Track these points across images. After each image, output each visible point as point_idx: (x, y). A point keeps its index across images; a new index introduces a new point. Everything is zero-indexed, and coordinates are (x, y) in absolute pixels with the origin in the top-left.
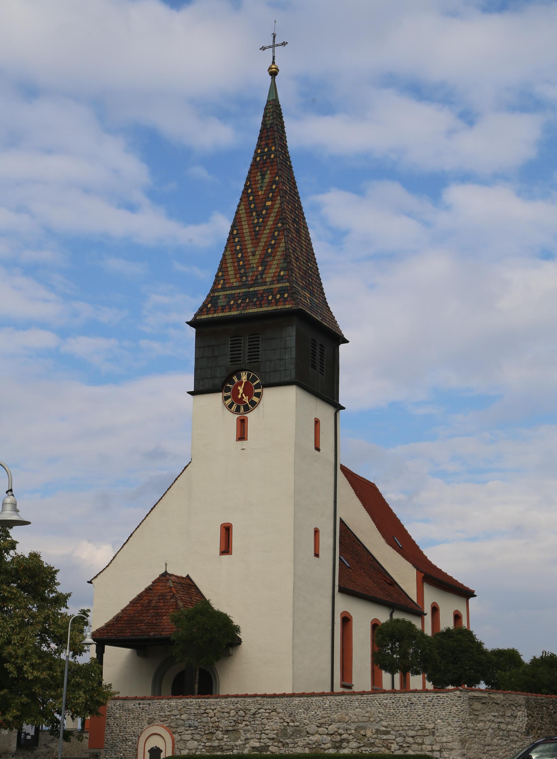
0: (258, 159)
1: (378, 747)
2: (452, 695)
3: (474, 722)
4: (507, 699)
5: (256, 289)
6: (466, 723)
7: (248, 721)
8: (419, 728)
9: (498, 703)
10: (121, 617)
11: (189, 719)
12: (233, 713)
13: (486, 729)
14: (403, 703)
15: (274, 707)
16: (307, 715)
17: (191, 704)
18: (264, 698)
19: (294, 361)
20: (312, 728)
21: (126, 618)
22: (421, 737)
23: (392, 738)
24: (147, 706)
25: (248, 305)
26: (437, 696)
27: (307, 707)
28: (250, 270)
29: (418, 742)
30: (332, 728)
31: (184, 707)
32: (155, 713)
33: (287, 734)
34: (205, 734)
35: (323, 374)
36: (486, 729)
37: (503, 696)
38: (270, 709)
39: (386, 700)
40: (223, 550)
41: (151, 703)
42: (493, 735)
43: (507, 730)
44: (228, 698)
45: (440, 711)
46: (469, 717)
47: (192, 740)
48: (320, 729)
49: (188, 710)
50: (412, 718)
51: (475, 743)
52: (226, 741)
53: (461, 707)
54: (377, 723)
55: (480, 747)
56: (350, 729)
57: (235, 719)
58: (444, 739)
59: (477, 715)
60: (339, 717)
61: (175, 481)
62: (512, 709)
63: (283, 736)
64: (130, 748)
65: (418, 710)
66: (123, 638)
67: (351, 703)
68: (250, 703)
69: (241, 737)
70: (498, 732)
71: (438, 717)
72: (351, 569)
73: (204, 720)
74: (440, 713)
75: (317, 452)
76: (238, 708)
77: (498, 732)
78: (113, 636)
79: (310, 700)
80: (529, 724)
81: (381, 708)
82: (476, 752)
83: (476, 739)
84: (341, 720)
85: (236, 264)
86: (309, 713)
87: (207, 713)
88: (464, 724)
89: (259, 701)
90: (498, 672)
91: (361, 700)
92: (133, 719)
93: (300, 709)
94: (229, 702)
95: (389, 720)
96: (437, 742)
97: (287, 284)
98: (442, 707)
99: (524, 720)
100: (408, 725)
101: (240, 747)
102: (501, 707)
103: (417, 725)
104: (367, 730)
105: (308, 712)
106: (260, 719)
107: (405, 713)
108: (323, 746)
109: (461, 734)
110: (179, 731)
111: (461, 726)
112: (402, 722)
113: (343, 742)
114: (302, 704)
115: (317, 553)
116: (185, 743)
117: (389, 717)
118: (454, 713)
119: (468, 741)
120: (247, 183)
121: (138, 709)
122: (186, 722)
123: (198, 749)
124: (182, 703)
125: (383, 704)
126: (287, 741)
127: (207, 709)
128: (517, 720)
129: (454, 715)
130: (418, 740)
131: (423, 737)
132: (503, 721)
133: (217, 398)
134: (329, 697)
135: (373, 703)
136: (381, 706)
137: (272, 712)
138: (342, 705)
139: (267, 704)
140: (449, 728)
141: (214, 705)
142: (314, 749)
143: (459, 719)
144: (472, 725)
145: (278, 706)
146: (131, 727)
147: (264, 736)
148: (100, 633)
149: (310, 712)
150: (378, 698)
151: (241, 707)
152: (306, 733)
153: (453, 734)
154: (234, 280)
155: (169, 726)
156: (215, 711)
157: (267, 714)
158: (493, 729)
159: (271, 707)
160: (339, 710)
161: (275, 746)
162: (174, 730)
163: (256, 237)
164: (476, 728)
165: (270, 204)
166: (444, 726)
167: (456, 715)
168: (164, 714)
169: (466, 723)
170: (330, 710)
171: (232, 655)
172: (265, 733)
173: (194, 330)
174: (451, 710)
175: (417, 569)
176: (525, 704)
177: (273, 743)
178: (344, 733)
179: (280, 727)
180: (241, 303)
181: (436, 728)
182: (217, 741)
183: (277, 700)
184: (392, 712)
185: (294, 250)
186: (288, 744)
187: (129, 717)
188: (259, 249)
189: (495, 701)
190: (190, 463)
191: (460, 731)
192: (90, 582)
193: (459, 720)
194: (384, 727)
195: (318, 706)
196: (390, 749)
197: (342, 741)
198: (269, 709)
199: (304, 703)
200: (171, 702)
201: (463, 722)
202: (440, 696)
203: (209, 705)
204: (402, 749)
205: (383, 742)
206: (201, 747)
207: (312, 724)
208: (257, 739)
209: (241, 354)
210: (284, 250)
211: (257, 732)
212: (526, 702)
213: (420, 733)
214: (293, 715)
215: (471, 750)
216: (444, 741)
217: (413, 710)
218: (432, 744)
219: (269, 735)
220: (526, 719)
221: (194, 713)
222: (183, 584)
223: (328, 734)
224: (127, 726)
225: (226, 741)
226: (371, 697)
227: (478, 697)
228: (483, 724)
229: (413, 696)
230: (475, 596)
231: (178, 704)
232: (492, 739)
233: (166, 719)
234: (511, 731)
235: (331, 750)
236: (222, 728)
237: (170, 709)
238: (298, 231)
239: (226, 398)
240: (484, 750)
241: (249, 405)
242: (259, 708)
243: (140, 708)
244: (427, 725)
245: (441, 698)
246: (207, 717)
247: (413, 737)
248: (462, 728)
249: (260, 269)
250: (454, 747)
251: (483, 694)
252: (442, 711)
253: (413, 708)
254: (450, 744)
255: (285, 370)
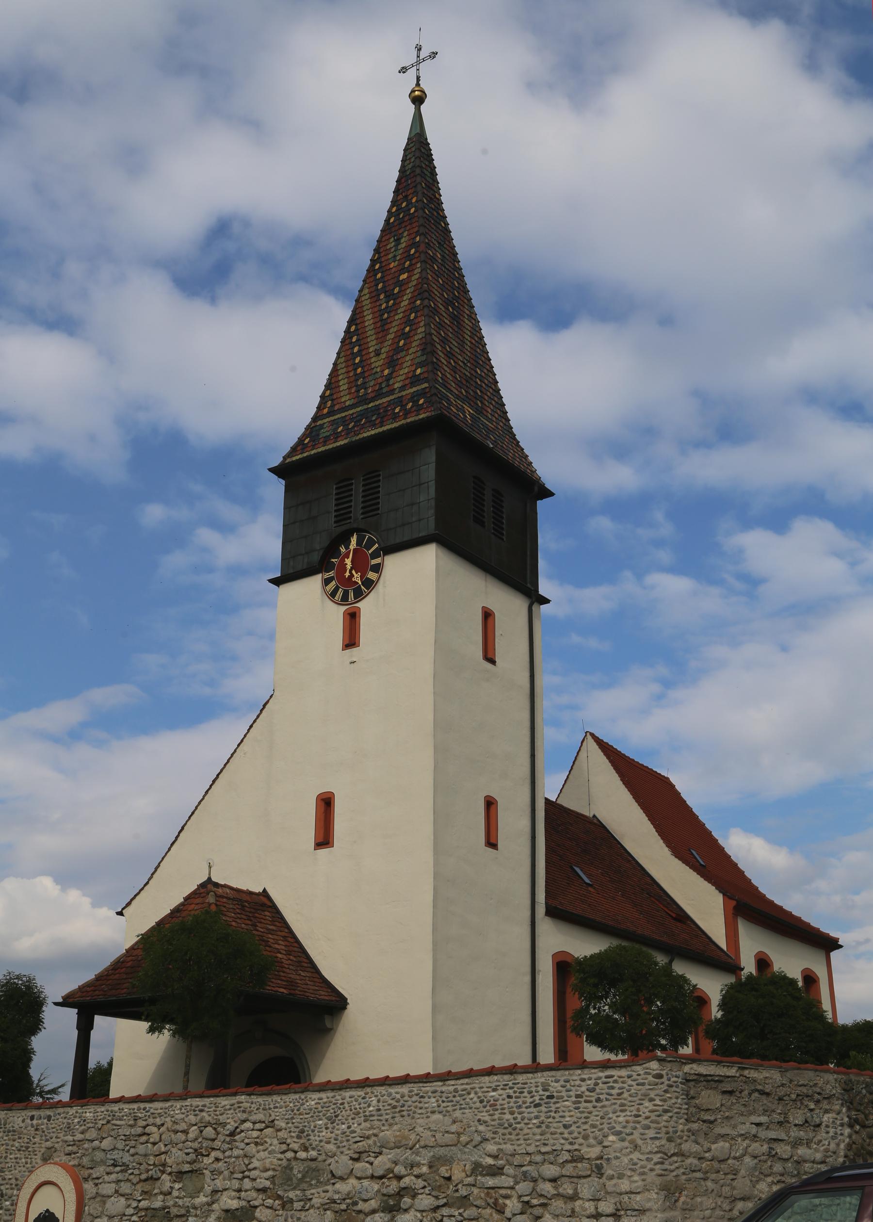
0: (392, 220)
1: (476, 1206)
2: (642, 1072)
3: (701, 1140)
4: (791, 1081)
5: (377, 403)
6: (679, 1141)
7: (219, 1149)
8: (566, 1156)
9: (768, 1091)
10: (123, 962)
11: (114, 1149)
12: (193, 1132)
13: (735, 1158)
14: (532, 1097)
15: (270, 1115)
16: (332, 1133)
17: (121, 1114)
18: (252, 1097)
19: (433, 503)
20: (342, 1163)
21: (129, 964)
22: (572, 1180)
23: (506, 1185)
24: (45, 1121)
25: (363, 427)
26: (607, 1077)
27: (333, 1115)
28: (371, 378)
29: (564, 1192)
30: (382, 1163)
31: (108, 1122)
32: (57, 1137)
33: (291, 1179)
34: (140, 1181)
35: (503, 539)
36: (735, 1158)
37: (779, 1075)
38: (264, 1122)
39: (494, 1090)
40: (321, 840)
41: (52, 1115)
42: (757, 1173)
43: (795, 1158)
44: (186, 1099)
45: (614, 1113)
46: (687, 1127)
47: (116, 1195)
48: (358, 1165)
49: (114, 1129)
50: (552, 1134)
51: (706, 1193)
52: (177, 1197)
53: (665, 1101)
54: (475, 1147)
55: (719, 1203)
56: (419, 1165)
57: (196, 1145)
58: (625, 1185)
59: (711, 1122)
60: (397, 1136)
61: (249, 730)
62: (807, 1106)
63: (285, 1184)
64: (6, 1215)
65: (564, 1112)
66: (114, 998)
67: (420, 1102)
68: (226, 1110)
69: (206, 1186)
70: (769, 1163)
71: (608, 1128)
72: (595, 888)
73: (141, 1149)
74: (614, 1118)
75: (489, 666)
76: (203, 1121)
77: (769, 1163)
78: (100, 997)
79: (338, 1096)
80: (854, 1143)
81: (485, 1110)
82: (710, 1217)
83: (709, 1184)
84: (400, 1142)
85: (351, 374)
86: (337, 1127)
87: (149, 1135)
88: (673, 1144)
89: (242, 1103)
90: (850, 1054)
91: (442, 1092)
92: (19, 1150)
93: (320, 1120)
94: (189, 1108)
95: (501, 1141)
96: (607, 1193)
97: (426, 385)
98: (619, 1102)
99: (842, 1134)
100: (543, 1149)
101: (202, 1209)
102: (776, 1102)
103: (562, 1149)
104: (454, 1166)
105: (335, 1124)
106: (242, 1145)
107: (535, 1121)
108: (361, 1206)
109: (666, 1170)
110: (94, 1176)
111: (663, 1149)
112: (529, 1145)
113: (403, 1196)
114: (322, 1108)
115: (492, 841)
116: (104, 1203)
117: (501, 1131)
118: (647, 1118)
119: (686, 1188)
120: (375, 256)
121: (29, 1128)
122: (108, 1156)
123: (124, 1215)
124: (105, 1113)
125: (488, 1101)
126: (291, 1194)
127: (148, 1125)
128: (822, 1134)
129: (647, 1122)
130: (565, 1189)
131: (575, 1180)
132: (783, 1136)
133: (316, 581)
134: (377, 1088)
135: (468, 1100)
136: (485, 1107)
137: (267, 1127)
138: (401, 1107)
139: (257, 1109)
140: (635, 1156)
141: (160, 1117)
142: (343, 1213)
143: (659, 1133)
144: (695, 1148)
145: (277, 1114)
146: (13, 1168)
147: (247, 1183)
148: (83, 992)
149: (338, 1125)
150: (476, 1086)
151: (210, 1118)
152: (330, 1176)
153: (646, 1170)
154: (348, 397)
155: (79, 1165)
156: (162, 1129)
157: (255, 1134)
158: (755, 1157)
159: (265, 1115)
160: (397, 1120)
161: (267, 1207)
162: (86, 1173)
163: (382, 327)
164: (707, 1155)
165: (406, 277)
166: (624, 1151)
167: (651, 1122)
168: (71, 1138)
169: (679, 1141)
170: (378, 1120)
171: (331, 1029)
172: (249, 1177)
173: (283, 482)
174: (638, 1110)
175: (724, 895)
176: (841, 1094)
177: (264, 1200)
178: (406, 1173)
179: (280, 1162)
180: (354, 427)
181: (606, 1157)
182: (160, 1197)
183: (276, 1101)
184: (507, 1120)
185: (444, 341)
186: (291, 1201)
187: (12, 1146)
188: (386, 344)
189: (760, 1087)
190: (271, 696)
191: (662, 1163)
192: (120, 913)
193: (658, 1136)
194: (490, 1156)
195: (354, 1111)
196: (503, 1213)
197: (401, 1193)
198: (260, 1122)
199: (327, 1105)
200: (86, 1112)
201: (670, 1140)
202: (612, 1076)
203: (151, 1116)
204: (528, 1212)
205: (488, 1194)
206: (130, 1211)
207: (342, 1153)
208: (235, 1191)
209: (351, 506)
210: (423, 337)
211: (236, 1176)
212: (844, 1090)
213: (569, 1169)
214: (305, 1134)
215: (696, 1213)
216: (623, 1190)
217: (552, 1114)
218: (597, 1198)
219: (258, 1180)
220: (847, 1131)
221: (124, 1135)
222: (246, 901)
223: (372, 1177)
224: (7, 1165)
225: (177, 1197)
226: (462, 1084)
227: (710, 1075)
228: (727, 1145)
229: (553, 1079)
230: (841, 947)
231: (97, 1116)
232: (754, 1184)
233: (75, 1149)
234: (805, 1161)
235: (377, 1215)
236: (171, 1167)
237: (83, 1127)
238: (456, 319)
239: (327, 582)
240: (731, 1210)
241: (362, 587)
242: (243, 1119)
243: (32, 1126)
244: (584, 1150)
245: (615, 1082)
246: (147, 1142)
247: (553, 1180)
248: (666, 1154)
249: (386, 372)
250: (648, 1205)
251: (725, 1069)
252: (618, 1114)
253: (553, 1109)
254: (638, 1198)
255: (420, 520)
